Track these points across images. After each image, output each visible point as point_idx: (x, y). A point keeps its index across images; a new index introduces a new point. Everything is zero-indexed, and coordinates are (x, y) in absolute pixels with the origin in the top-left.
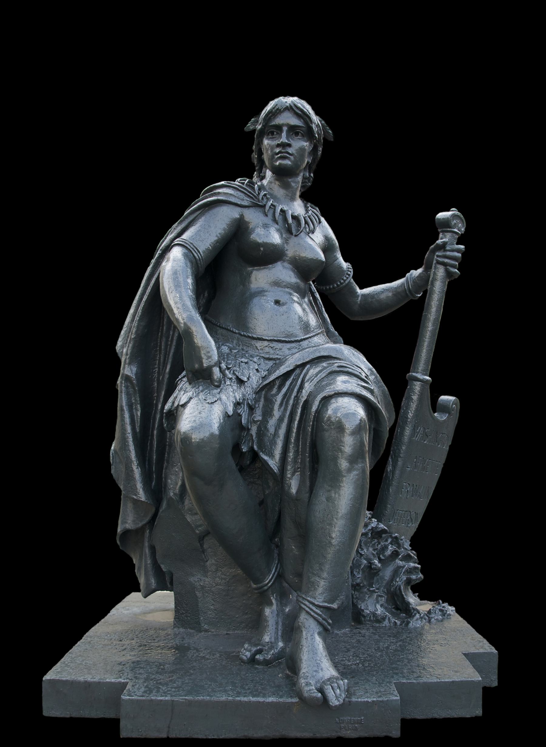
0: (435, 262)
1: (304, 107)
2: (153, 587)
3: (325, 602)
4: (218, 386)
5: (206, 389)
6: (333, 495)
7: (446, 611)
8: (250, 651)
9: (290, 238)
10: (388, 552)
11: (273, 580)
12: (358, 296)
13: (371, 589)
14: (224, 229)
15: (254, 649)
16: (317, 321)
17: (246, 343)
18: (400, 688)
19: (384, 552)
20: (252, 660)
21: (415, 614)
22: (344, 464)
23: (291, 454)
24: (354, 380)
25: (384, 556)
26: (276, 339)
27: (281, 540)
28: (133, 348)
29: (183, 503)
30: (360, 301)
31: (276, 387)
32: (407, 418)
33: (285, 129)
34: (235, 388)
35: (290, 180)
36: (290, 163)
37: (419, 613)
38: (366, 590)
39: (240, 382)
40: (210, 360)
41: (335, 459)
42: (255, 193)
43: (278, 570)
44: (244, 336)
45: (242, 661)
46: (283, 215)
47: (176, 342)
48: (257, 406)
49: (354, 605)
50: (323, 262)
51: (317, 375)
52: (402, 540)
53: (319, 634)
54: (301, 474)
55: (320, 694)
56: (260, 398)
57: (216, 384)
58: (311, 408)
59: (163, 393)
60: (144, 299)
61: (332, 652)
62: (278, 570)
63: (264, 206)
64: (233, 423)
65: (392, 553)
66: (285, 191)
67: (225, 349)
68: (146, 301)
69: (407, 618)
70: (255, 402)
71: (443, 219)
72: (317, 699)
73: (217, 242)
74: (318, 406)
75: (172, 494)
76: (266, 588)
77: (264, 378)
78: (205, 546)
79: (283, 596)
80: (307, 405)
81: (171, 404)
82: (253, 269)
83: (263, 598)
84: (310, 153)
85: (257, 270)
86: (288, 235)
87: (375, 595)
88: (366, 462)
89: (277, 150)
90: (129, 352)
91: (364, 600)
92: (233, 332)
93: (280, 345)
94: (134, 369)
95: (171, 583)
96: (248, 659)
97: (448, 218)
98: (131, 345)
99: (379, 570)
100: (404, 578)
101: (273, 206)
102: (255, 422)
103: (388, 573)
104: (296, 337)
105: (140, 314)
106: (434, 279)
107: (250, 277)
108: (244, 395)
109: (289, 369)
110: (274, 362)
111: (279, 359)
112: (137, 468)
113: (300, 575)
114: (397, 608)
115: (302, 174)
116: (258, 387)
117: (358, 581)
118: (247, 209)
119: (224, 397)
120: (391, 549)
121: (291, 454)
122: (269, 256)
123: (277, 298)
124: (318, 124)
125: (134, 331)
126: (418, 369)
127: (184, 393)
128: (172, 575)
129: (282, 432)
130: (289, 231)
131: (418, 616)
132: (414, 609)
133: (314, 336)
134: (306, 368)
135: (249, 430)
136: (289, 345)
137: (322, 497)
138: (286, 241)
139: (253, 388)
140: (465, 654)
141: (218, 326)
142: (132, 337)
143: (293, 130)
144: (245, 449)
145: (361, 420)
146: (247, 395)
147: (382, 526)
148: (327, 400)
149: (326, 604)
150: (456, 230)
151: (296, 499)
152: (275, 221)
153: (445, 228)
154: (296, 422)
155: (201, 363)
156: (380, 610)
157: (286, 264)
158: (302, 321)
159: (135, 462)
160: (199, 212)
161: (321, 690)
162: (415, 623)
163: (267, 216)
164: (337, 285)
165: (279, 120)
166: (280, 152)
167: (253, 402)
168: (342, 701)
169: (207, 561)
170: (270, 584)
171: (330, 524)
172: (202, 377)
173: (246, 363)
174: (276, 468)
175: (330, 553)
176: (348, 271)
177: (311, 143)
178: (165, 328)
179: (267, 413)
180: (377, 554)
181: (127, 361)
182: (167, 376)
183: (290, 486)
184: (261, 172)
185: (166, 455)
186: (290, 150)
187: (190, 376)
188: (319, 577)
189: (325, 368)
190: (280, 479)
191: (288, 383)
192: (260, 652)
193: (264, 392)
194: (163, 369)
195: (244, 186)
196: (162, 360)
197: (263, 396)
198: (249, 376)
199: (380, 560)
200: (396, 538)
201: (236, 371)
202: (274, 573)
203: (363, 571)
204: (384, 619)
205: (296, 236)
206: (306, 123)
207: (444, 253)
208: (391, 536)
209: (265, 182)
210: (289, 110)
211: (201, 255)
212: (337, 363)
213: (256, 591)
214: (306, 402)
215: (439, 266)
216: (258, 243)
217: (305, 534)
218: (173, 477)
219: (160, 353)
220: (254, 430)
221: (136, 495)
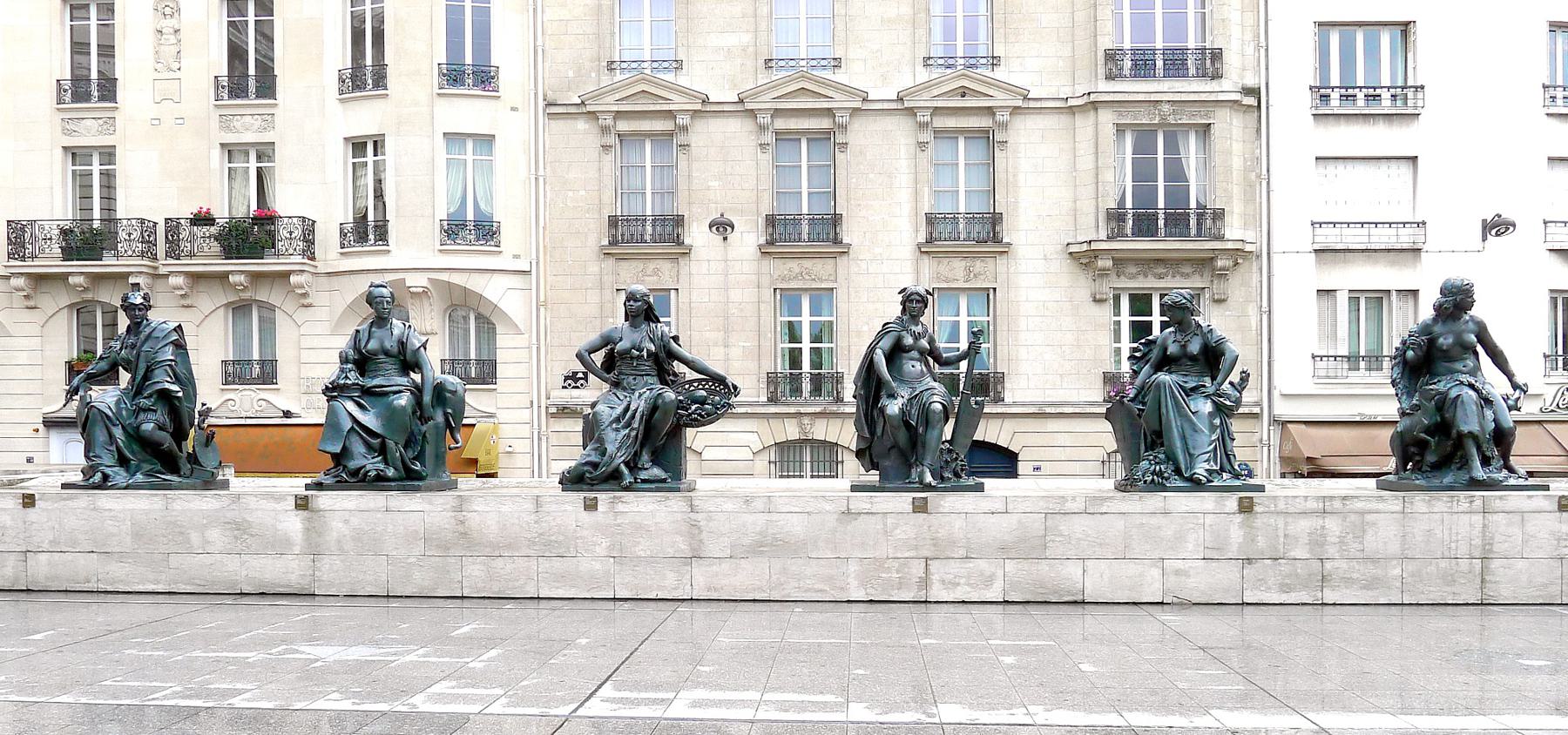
64: (902, 410)
83: (910, 467)
122: (908, 350)
127: (884, 401)
172: (892, 396)
190: (916, 429)
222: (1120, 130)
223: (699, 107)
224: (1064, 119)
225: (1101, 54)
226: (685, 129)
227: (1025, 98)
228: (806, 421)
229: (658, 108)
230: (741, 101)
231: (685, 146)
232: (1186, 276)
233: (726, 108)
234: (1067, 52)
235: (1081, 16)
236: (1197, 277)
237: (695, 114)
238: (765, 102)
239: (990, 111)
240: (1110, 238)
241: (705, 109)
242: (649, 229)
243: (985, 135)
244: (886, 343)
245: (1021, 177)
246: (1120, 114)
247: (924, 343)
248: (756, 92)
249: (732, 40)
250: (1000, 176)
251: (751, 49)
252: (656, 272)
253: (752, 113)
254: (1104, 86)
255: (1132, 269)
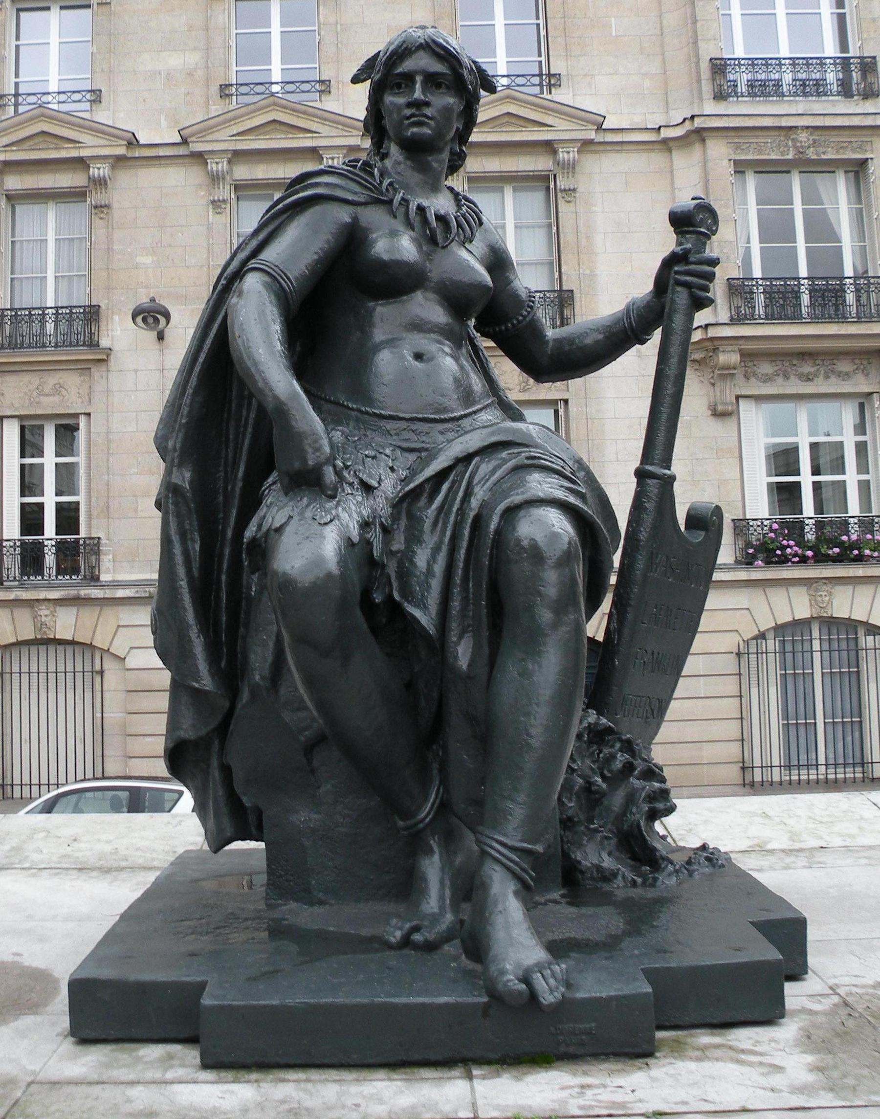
0: (672, 282)
1: (448, 43)
2: (229, 834)
3: (522, 841)
4: (333, 497)
5: (315, 500)
6: (530, 666)
7: (717, 859)
8: (400, 929)
9: (434, 252)
10: (618, 765)
11: (432, 813)
12: (548, 341)
13: (592, 826)
14: (328, 242)
15: (408, 926)
16: (484, 386)
17: (371, 425)
18: (651, 975)
19: (610, 765)
20: (406, 942)
21: (666, 866)
22: (546, 615)
23: (456, 604)
24: (554, 480)
25: (610, 771)
26: (420, 416)
27: (445, 748)
28: (186, 438)
29: (277, 692)
30: (552, 350)
31: (425, 495)
32: (639, 541)
33: (419, 79)
34: (359, 498)
35: (430, 158)
36: (429, 132)
37: (672, 863)
38: (582, 828)
39: (367, 489)
40: (318, 454)
41: (530, 609)
42: (375, 180)
43: (440, 796)
44: (367, 413)
45: (390, 947)
46: (420, 215)
47: (253, 428)
48: (395, 527)
49: (566, 855)
50: (489, 288)
51: (493, 472)
52: (637, 745)
53: (516, 893)
54: (474, 636)
55: (524, 986)
56: (399, 513)
57: (329, 493)
58: (488, 526)
59: (234, 512)
60: (201, 360)
61: (537, 927)
62: (440, 796)
63: (390, 202)
64: (361, 555)
65: (624, 766)
66: (421, 176)
67: (337, 436)
68: (204, 362)
69: (651, 872)
70: (393, 522)
71: (682, 212)
72: (520, 992)
73: (317, 262)
74: (499, 524)
75: (257, 677)
76: (421, 825)
77: (405, 481)
78: (315, 763)
79: (449, 839)
80: (479, 522)
81: (254, 529)
82: (376, 305)
83: (415, 845)
84: (460, 114)
85: (381, 305)
86: (431, 248)
87: (599, 836)
88: (581, 610)
89: (408, 112)
90: (178, 446)
91: (580, 846)
92: (348, 407)
93: (425, 427)
94: (188, 475)
95: (260, 827)
96: (398, 943)
97: (689, 211)
98: (181, 435)
99: (603, 794)
100: (646, 807)
101: (405, 202)
102: (392, 553)
103: (617, 800)
104: (452, 412)
105: (194, 383)
106: (673, 311)
107: (371, 316)
108: (374, 510)
109: (446, 464)
110: (418, 454)
111: (426, 450)
112: (199, 636)
113: (479, 803)
114: (634, 858)
115: (448, 148)
116: (397, 496)
117: (570, 813)
118: (363, 207)
119: (344, 516)
120: (621, 758)
121: (456, 604)
122: (397, 282)
123: (418, 350)
124: (472, 68)
125: (186, 412)
126: (653, 458)
127: (276, 510)
128: (259, 813)
129: (439, 568)
130: (432, 240)
131: (670, 868)
132: (664, 858)
133: (481, 410)
134: (474, 462)
135: (384, 566)
136: (440, 427)
137: (510, 670)
138: (428, 256)
139: (386, 498)
140: (751, 923)
141: (322, 399)
142: (183, 421)
143: (432, 81)
144: (378, 598)
145: (570, 543)
146: (379, 509)
147: (604, 721)
148: (512, 512)
149: (525, 845)
150: (702, 230)
151: (469, 677)
152: (410, 225)
153: (688, 226)
154: (463, 552)
155: (305, 461)
156: (608, 863)
157: (431, 296)
158: (461, 386)
159: (194, 627)
160: (285, 216)
161: (526, 980)
162: (667, 881)
163: (395, 217)
164: (513, 324)
165: (408, 65)
166: (412, 116)
167: (390, 522)
168: (559, 996)
169: (319, 787)
170: (428, 820)
171: (527, 714)
172: (308, 482)
173: (374, 458)
174: (432, 627)
175: (529, 763)
176: (530, 301)
177: (461, 97)
178: (233, 405)
179: (414, 538)
180: (598, 768)
181: (176, 461)
182: (240, 484)
183: (456, 658)
184: (382, 147)
185: (242, 616)
186: (428, 112)
187: (286, 481)
188: (512, 800)
189: (505, 461)
190: (439, 646)
191: (445, 487)
192: (416, 929)
193: (405, 505)
194: (232, 472)
195: (357, 171)
196: (230, 456)
197: (404, 511)
198: (380, 479)
199: (604, 777)
200: (629, 742)
201: (359, 470)
202: (434, 801)
203: (578, 797)
204: (614, 875)
205: (444, 247)
206: (452, 68)
207: (687, 268)
208: (620, 740)
209: (388, 163)
210: (424, 49)
211: (292, 284)
212: (525, 452)
213: (405, 833)
214: (478, 519)
215: (679, 289)
216: (384, 261)
217: (485, 733)
218: (259, 650)
219: (227, 447)
220: (392, 568)
221: (197, 682)
222: (740, 168)
223: (121, 151)
224: (657, 159)
225: (705, 66)
226: (101, 183)
227: (600, 128)
228: (44, 611)
229: (63, 154)
230: (185, 142)
231: (102, 208)
232: (845, 376)
233: (162, 152)
234: (655, 68)
235: (672, 19)
236: (860, 377)
237: (119, 161)
238: (222, 140)
239: (549, 147)
240: (735, 321)
241: (133, 154)
242: (50, 327)
243: (543, 180)
244: (297, 248)
245: (599, 239)
246: (737, 147)
247: (469, 261)
248: (206, 129)
249: (175, 61)
250: (567, 236)
251: (200, 73)
252: (59, 389)
253: (200, 157)
254: (710, 107)
255: (766, 368)
